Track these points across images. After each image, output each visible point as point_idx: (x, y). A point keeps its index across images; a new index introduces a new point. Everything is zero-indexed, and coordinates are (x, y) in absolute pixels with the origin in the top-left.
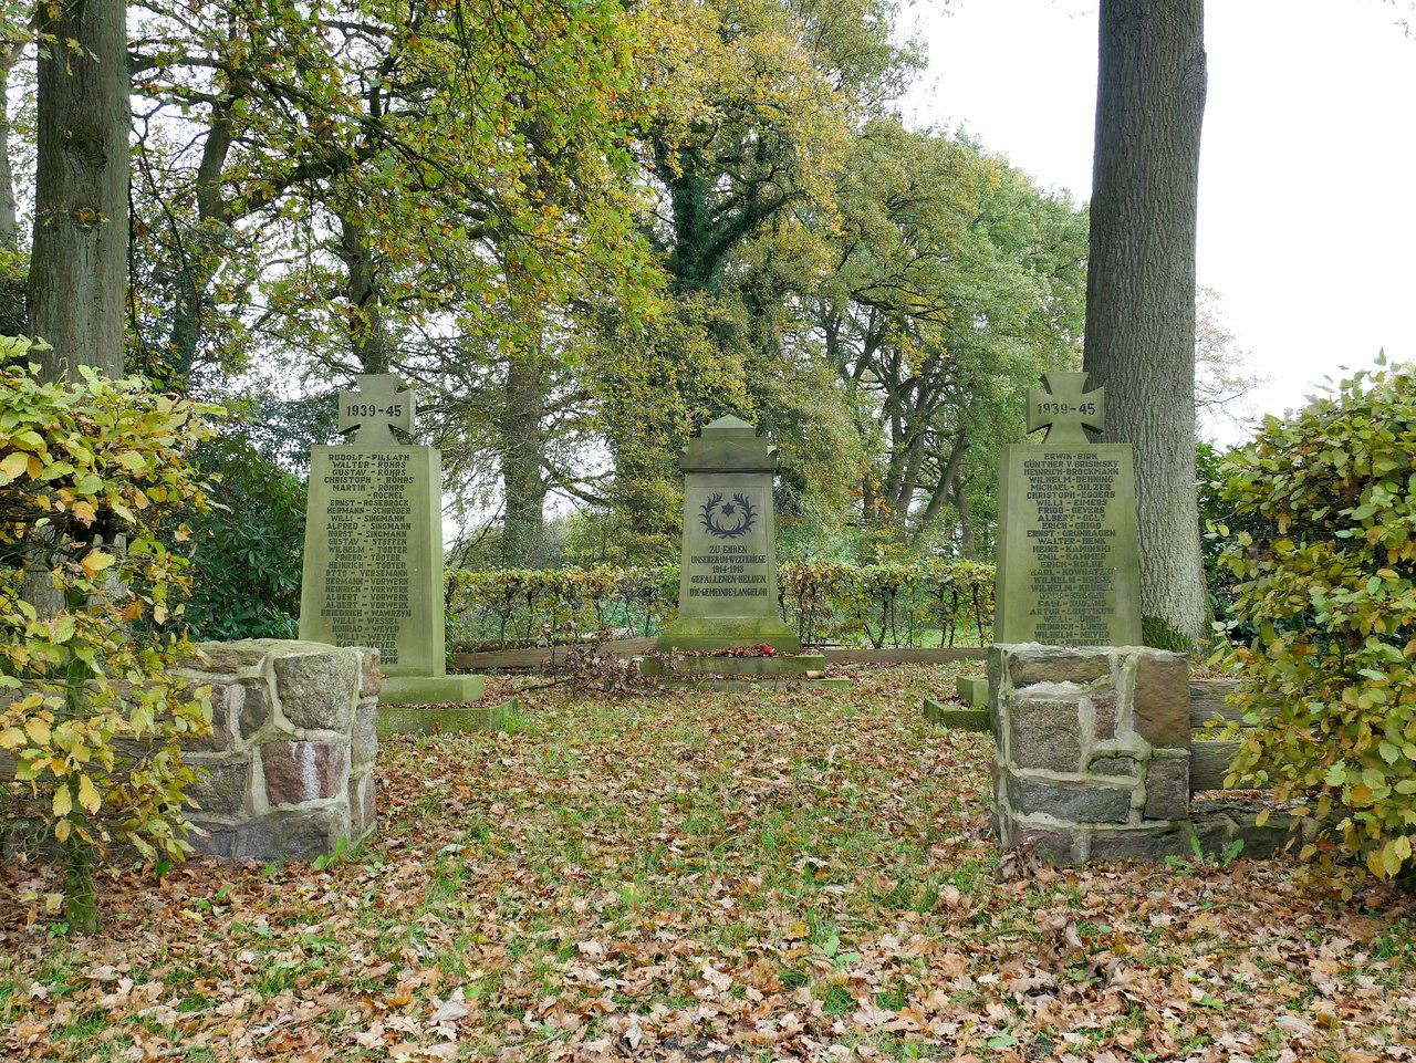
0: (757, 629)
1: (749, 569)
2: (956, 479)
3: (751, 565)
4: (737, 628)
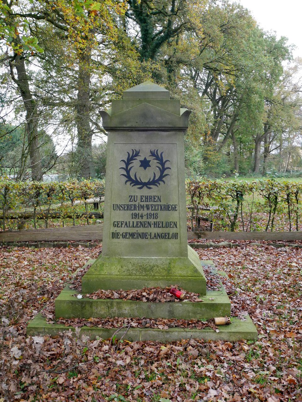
0: (169, 270)
1: (163, 216)
2: (232, 131)
3: (165, 213)
4: (152, 269)
